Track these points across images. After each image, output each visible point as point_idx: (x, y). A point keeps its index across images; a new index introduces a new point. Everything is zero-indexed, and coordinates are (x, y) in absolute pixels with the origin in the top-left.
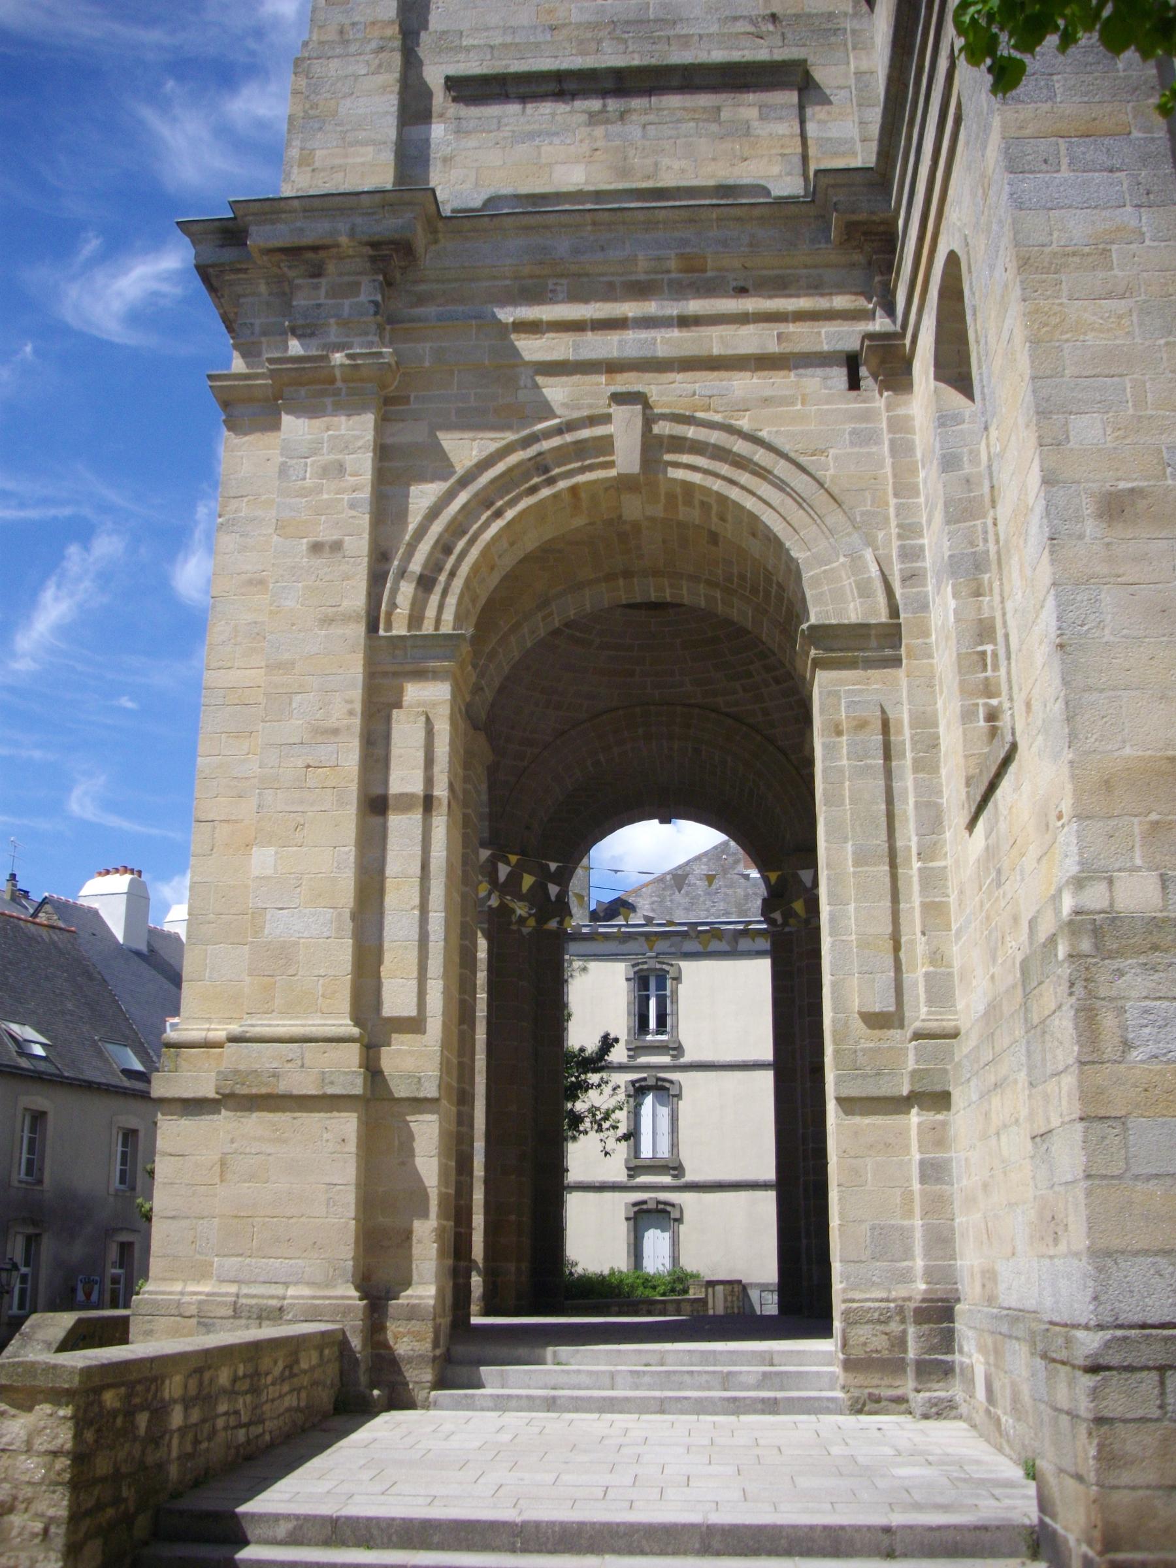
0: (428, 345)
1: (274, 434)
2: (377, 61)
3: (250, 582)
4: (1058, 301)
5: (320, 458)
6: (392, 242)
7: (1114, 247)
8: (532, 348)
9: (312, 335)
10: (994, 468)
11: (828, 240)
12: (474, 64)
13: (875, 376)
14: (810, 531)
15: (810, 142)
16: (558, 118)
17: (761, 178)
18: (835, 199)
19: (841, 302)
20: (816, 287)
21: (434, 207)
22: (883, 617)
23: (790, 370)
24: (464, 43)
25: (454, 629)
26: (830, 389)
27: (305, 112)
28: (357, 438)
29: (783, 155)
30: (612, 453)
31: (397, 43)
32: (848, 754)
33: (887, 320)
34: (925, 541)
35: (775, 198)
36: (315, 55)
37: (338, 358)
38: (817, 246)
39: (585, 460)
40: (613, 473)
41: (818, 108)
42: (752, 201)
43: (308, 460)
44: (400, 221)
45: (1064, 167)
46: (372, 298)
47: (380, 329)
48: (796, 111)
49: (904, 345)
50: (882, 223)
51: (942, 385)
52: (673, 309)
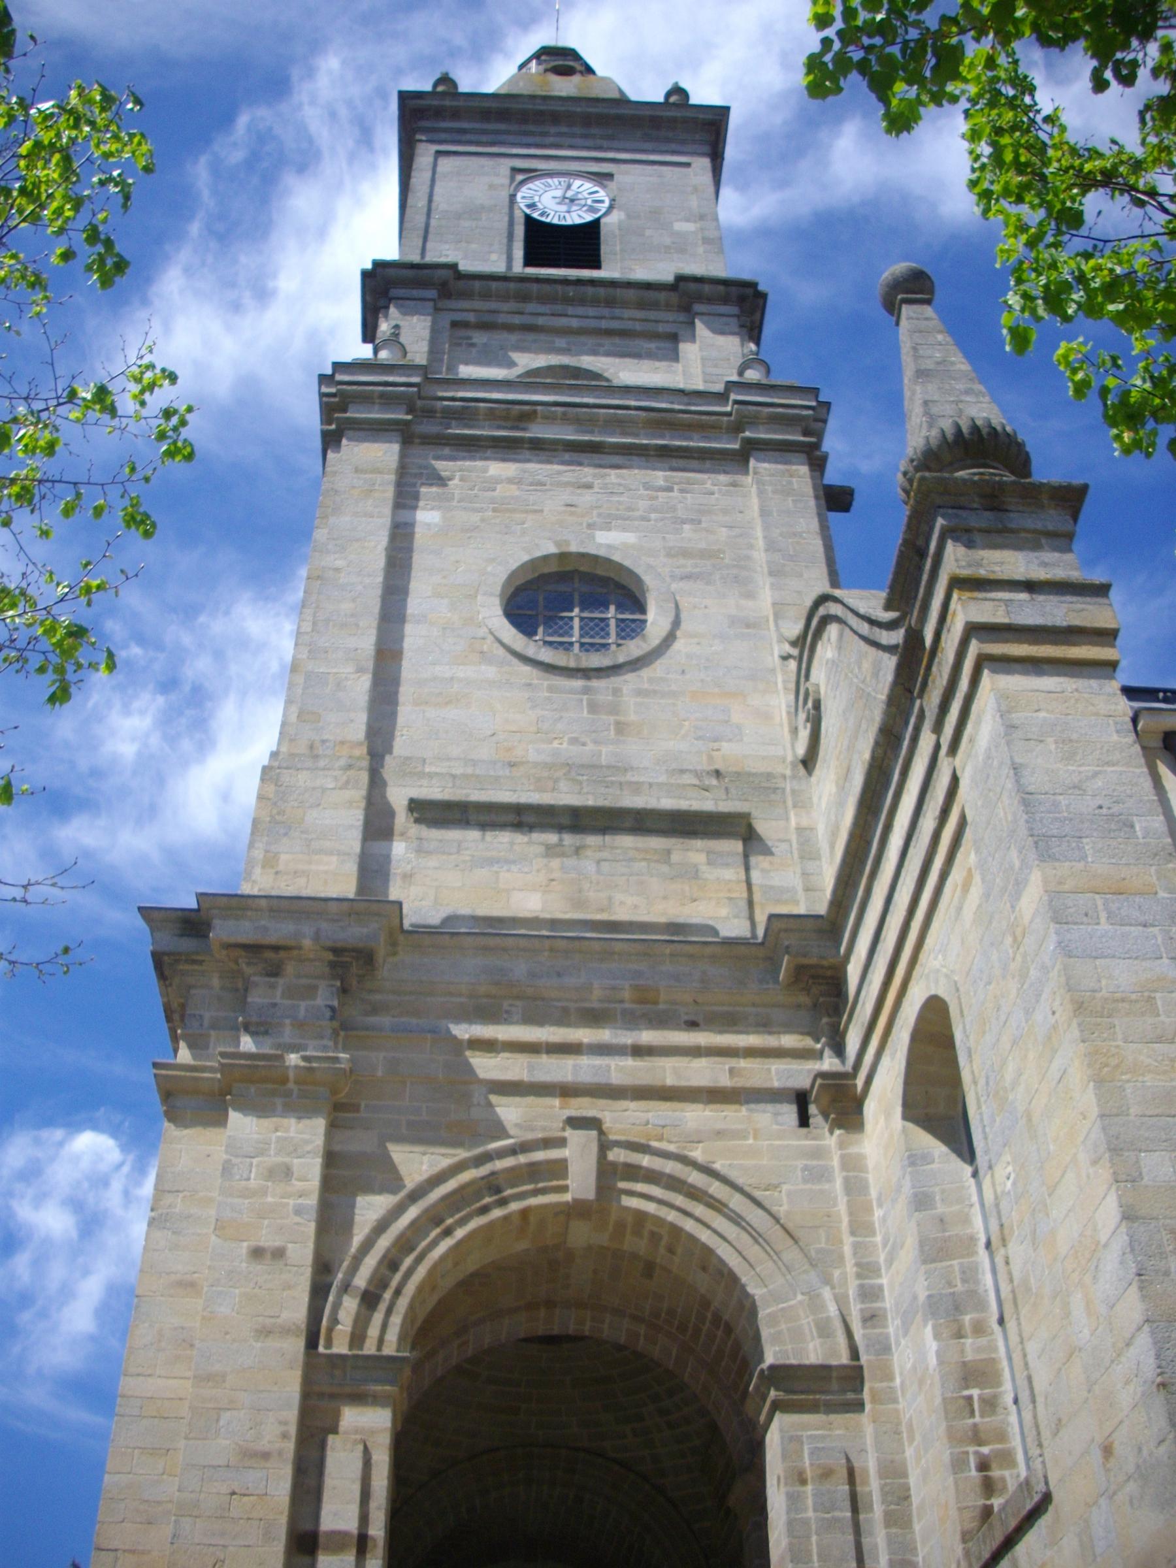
0: (382, 1055)
1: (222, 1130)
2: (345, 778)
3: (181, 1284)
4: (1114, 1043)
5: (266, 1159)
6: (354, 950)
7: (1158, 995)
8: (486, 1066)
9: (266, 1033)
10: (1002, 1206)
11: (776, 981)
12: (437, 790)
13: (826, 1116)
14: (766, 1267)
15: (755, 889)
16: (516, 847)
17: (711, 918)
18: (786, 943)
19: (789, 1041)
20: (765, 1025)
21: (398, 920)
22: (844, 1359)
23: (741, 1104)
24: (427, 770)
25: (398, 1351)
26: (781, 1124)
27: (272, 816)
28: (307, 1142)
29: (730, 899)
30: (565, 1176)
31: (365, 763)
32: (815, 1504)
33: (836, 1061)
34: (884, 1281)
35: (724, 938)
36: (285, 765)
37: (293, 1059)
38: (765, 986)
39: (537, 1182)
40: (568, 1197)
41: (761, 858)
42: (703, 939)
43: (255, 1161)
44: (365, 930)
45: (1103, 920)
46: (330, 1003)
47: (335, 1033)
48: (740, 859)
49: (855, 1086)
50: (830, 968)
51: (910, 1125)
52: (627, 1038)
